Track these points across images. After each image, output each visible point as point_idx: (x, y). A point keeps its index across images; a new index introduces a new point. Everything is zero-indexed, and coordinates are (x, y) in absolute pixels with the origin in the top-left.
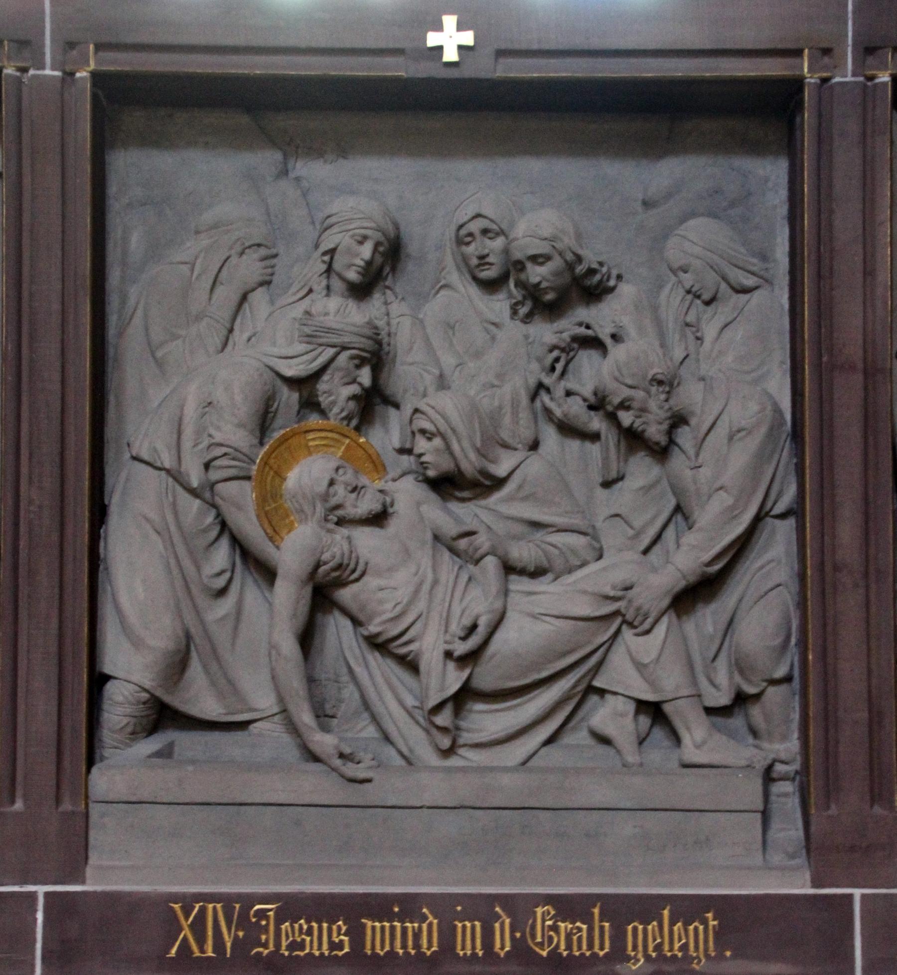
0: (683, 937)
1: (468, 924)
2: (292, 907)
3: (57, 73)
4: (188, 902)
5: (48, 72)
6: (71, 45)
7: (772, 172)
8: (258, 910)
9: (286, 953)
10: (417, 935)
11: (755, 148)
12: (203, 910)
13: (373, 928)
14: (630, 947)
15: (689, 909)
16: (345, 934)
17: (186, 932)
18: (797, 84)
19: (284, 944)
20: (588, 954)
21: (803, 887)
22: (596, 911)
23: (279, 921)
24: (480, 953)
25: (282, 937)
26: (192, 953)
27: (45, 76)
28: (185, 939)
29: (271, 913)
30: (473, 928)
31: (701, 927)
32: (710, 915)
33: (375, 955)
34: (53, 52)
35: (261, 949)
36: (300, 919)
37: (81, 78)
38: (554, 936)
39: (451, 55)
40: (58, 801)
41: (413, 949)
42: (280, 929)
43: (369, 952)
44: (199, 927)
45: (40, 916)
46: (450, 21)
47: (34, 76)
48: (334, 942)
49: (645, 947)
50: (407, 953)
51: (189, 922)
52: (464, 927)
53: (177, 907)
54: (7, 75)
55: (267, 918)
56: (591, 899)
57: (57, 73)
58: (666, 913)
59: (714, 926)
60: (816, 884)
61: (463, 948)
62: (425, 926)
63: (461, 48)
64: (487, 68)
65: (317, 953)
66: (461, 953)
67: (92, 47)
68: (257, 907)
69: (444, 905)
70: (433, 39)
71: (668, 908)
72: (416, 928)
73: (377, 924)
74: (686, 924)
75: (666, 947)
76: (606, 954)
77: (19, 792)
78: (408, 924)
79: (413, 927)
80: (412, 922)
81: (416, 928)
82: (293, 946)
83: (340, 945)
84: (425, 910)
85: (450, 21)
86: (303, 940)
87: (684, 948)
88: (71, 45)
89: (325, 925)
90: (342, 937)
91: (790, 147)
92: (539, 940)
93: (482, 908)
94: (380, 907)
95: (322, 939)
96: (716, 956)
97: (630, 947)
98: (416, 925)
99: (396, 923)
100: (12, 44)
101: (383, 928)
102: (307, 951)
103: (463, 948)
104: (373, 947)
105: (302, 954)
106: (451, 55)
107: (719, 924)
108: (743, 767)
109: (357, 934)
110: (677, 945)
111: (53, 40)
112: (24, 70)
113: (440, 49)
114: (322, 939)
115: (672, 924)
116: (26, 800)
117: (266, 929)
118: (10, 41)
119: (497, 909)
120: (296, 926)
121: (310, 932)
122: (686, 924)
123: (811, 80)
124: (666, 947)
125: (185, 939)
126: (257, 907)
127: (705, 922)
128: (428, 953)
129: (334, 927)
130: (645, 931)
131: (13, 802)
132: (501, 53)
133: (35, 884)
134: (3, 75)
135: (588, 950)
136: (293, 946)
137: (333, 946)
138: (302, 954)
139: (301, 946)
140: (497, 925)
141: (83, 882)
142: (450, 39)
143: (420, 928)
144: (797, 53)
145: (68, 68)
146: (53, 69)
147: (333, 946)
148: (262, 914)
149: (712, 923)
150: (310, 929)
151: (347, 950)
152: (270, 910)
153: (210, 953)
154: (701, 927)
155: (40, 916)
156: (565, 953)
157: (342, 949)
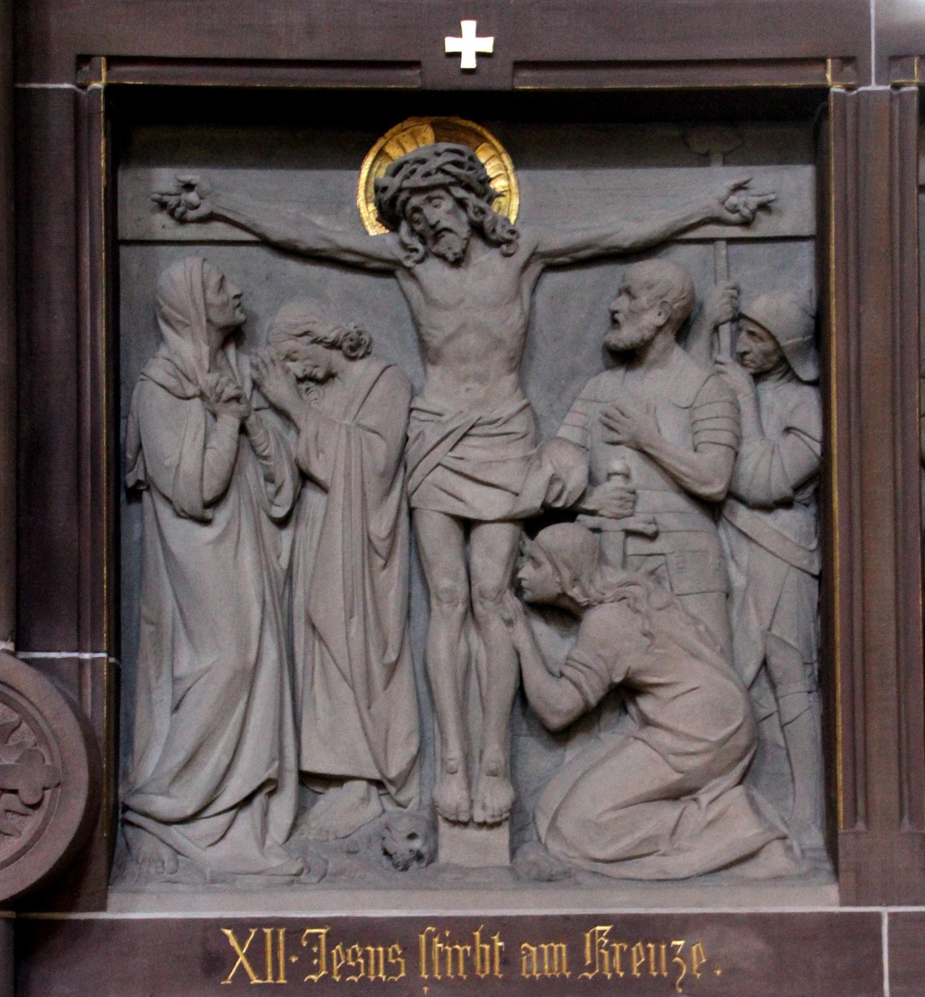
0: (342, 957)
1: (370, 949)
2: (344, 931)
4: (241, 927)
7: (805, 174)
8: (310, 934)
11: (783, 156)
12: (261, 937)
14: (479, 967)
16: (402, 956)
17: (242, 958)
18: (824, 91)
19: (336, 967)
20: (558, 975)
21: (831, 905)
23: (330, 946)
24: (665, 974)
28: (241, 965)
29: (323, 937)
30: (560, 949)
32: (496, 938)
33: (543, 978)
35: (586, 974)
36: (394, 943)
38: (608, 960)
39: (469, 62)
41: (655, 970)
42: (332, 955)
43: (609, 976)
44: (256, 955)
46: (469, 26)
48: (390, 963)
50: (615, 975)
51: (244, 951)
52: (377, 953)
53: (228, 932)
54: (835, 93)
56: (474, 922)
59: (500, 947)
60: (843, 903)
64: (500, 80)
65: (372, 978)
66: (372, 978)
68: (308, 931)
70: (451, 44)
73: (556, 947)
75: (652, 967)
78: (543, 946)
79: (465, 951)
80: (461, 945)
82: (346, 971)
84: (477, 934)
85: (469, 26)
88: (894, 59)
90: (399, 959)
91: (817, 155)
92: (588, 962)
97: (479, 967)
98: (625, 947)
99: (457, 947)
100: (837, 61)
104: (560, 969)
105: (356, 979)
106: (469, 62)
107: (506, 945)
109: (576, 951)
113: (458, 55)
117: (318, 955)
118: (833, 58)
120: (390, 950)
123: (836, 89)
126: (308, 931)
127: (492, 943)
128: (482, 976)
132: (519, 65)
135: (538, 972)
136: (346, 971)
138: (590, 976)
139: (356, 971)
141: (103, 907)
144: (822, 61)
146: (878, 82)
148: (314, 939)
150: (366, 955)
151: (403, 974)
152: (320, 934)
156: (655, 974)
157: (399, 972)
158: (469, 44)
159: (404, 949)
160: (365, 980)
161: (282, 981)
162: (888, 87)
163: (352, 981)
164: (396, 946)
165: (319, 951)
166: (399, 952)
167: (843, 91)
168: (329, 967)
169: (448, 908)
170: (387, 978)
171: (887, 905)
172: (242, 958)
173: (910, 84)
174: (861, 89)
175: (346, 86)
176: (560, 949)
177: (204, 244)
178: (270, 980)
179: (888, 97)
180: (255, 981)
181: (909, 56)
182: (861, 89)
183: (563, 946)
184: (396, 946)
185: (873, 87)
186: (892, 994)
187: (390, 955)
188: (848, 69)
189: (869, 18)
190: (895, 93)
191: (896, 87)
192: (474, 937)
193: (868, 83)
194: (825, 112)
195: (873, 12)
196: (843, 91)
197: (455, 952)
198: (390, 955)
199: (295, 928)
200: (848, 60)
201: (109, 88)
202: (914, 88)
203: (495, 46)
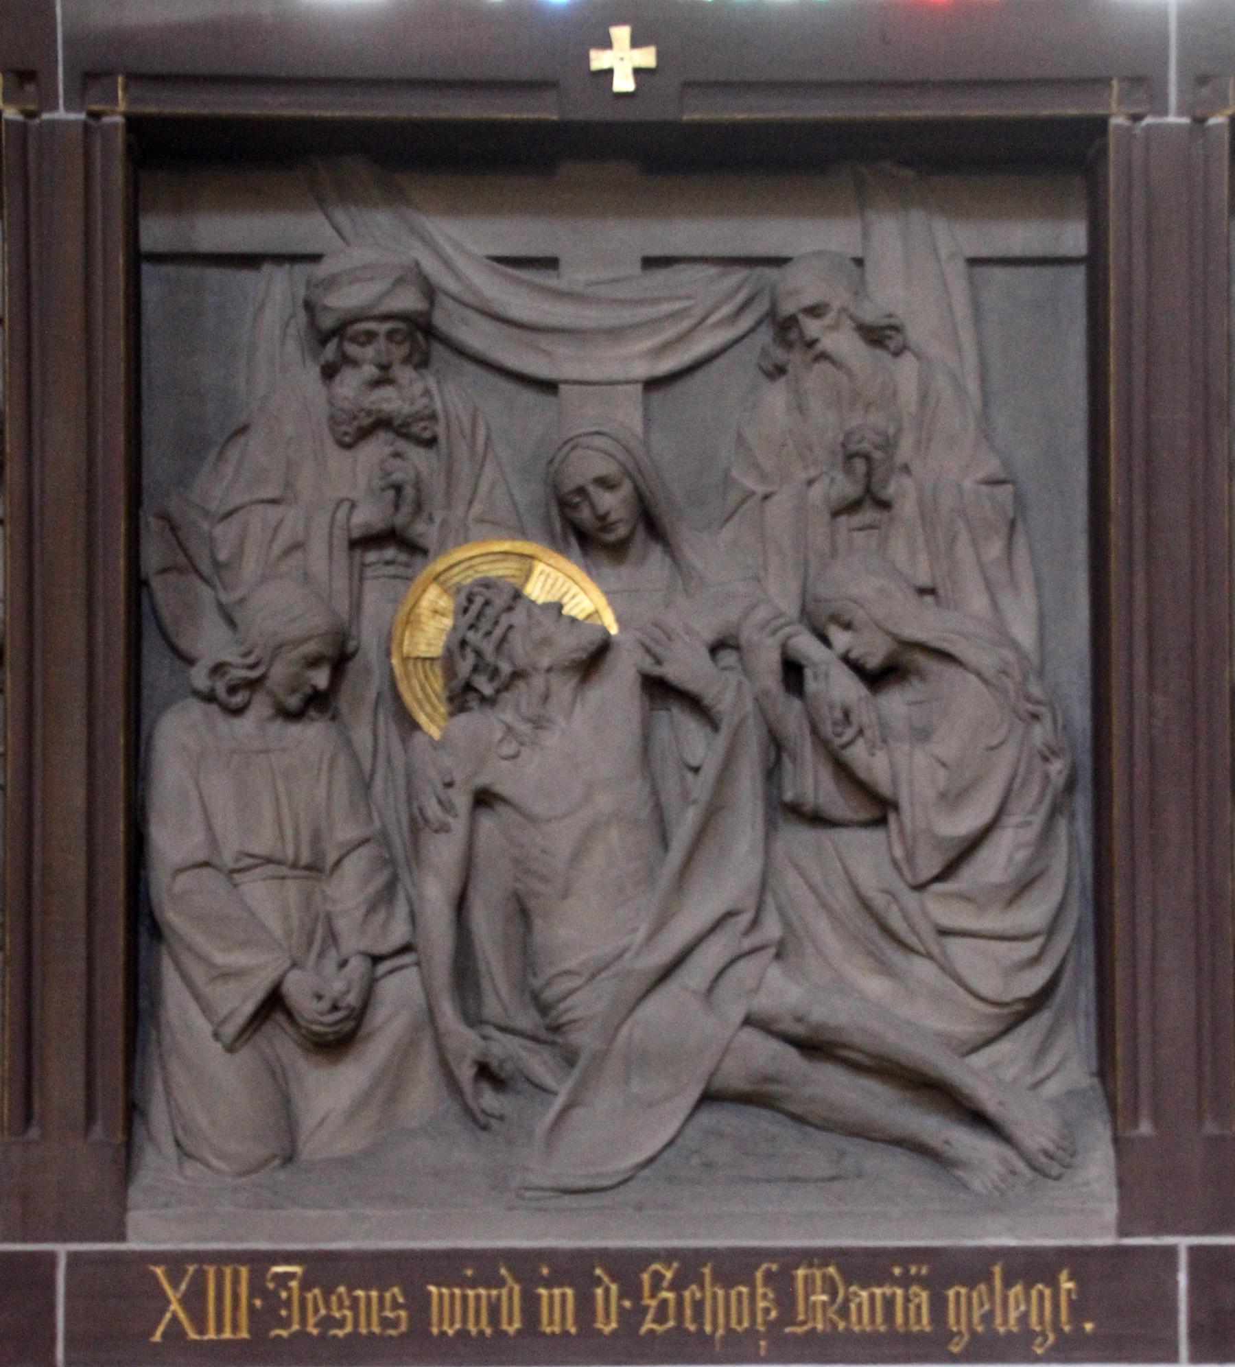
2: (325, 1269)
3: (1185, 120)
5: (1172, 119)
6: (1203, 80)
9: (315, 1332)
10: (698, 1306)
12: (200, 1276)
13: (441, 1296)
15: (1032, 1267)
17: (175, 1306)
18: (1100, 125)
22: (707, 1271)
23: (306, 1286)
24: (573, 1330)
25: (452, 1309)
26: (186, 1334)
27: (1168, 125)
28: (175, 1319)
30: (564, 1296)
31: (1047, 1292)
34: (1181, 92)
36: (337, 1286)
37: (1217, 126)
39: (624, 83)
40: (1200, 1120)
44: (194, 1301)
45: (1183, 1279)
47: (1149, 127)
49: (970, 1319)
52: (369, 1299)
53: (159, 1271)
54: (1118, 127)
55: (289, 1289)
57: (1185, 120)
58: (997, 1270)
59: (1069, 1291)
61: (551, 1322)
62: (504, 1292)
63: (638, 72)
64: (653, 112)
66: (1002, 1330)
67: (120, 79)
69: (524, 1264)
70: (599, 60)
71: (709, 1265)
72: (493, 1300)
74: (328, 1292)
76: (519, 1332)
77: (1145, 1111)
80: (438, 1285)
81: (493, 1300)
82: (328, 1322)
83: (394, 1323)
84: (598, 1272)
86: (344, 1318)
87: (1024, 1318)
88: (1203, 80)
89: (374, 1294)
92: (801, 1317)
93: (575, 1269)
94: (447, 1267)
95: (372, 1310)
96: (578, 1335)
97: (435, 1319)
101: (452, 1296)
102: (296, 1327)
103: (551, 1322)
105: (284, 1333)
106: (624, 83)
108: (721, 1060)
110: (976, 1315)
111: (1181, 73)
112: (1136, 118)
113: (609, 72)
114: (372, 1310)
115: (1008, 1284)
116: (1156, 1118)
117: (288, 1304)
119: (503, 1271)
120: (388, 1295)
121: (354, 1306)
122: (328, 1292)
123: (1118, 121)
124: (1034, 1318)
125: (175, 1319)
129: (975, 1295)
130: (969, 1299)
131: (1136, 1124)
133: (55, 1240)
134: (1111, 128)
137: (386, 1323)
138: (284, 1333)
140: (599, 1291)
141: (122, 1237)
142: (622, 60)
143: (499, 1297)
144: (1105, 82)
145: (1199, 113)
147: (386, 1323)
149: (1067, 1285)
152: (292, 1276)
153: (244, 1334)
154: (1047, 1292)
155: (1183, 1279)
158: (622, 60)
159: (405, 1293)
160: (355, 1334)
161: (244, 1334)
162: (82, 116)
163: (279, 1336)
164: (396, 1290)
165: (289, 1298)
166: (401, 1300)
167: (20, 118)
168: (303, 1321)
169: (536, 1238)
170: (764, 1338)
171: (65, 1240)
172: (175, 1306)
173: (113, 113)
174: (46, 116)
175: (316, 113)
176: (564, 1296)
177: (280, 1017)
178: (211, 1335)
179: (80, 130)
180: (193, 1335)
181: (111, 74)
182: (46, 116)
183: (569, 1292)
184: (396, 1290)
185: (61, 114)
186: (68, 1362)
187: (388, 1303)
188: (30, 88)
189: (54, 17)
190: (92, 122)
191: (95, 115)
192: (702, 1275)
193: (55, 107)
194: (1103, 151)
195: (59, 10)
196: (20, 118)
197: (478, 1297)
198: (388, 1303)
199: (259, 1261)
200: (1137, 81)
201: (134, 124)
202: (119, 119)
203: (659, 56)
